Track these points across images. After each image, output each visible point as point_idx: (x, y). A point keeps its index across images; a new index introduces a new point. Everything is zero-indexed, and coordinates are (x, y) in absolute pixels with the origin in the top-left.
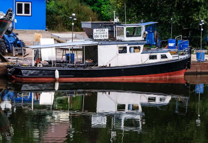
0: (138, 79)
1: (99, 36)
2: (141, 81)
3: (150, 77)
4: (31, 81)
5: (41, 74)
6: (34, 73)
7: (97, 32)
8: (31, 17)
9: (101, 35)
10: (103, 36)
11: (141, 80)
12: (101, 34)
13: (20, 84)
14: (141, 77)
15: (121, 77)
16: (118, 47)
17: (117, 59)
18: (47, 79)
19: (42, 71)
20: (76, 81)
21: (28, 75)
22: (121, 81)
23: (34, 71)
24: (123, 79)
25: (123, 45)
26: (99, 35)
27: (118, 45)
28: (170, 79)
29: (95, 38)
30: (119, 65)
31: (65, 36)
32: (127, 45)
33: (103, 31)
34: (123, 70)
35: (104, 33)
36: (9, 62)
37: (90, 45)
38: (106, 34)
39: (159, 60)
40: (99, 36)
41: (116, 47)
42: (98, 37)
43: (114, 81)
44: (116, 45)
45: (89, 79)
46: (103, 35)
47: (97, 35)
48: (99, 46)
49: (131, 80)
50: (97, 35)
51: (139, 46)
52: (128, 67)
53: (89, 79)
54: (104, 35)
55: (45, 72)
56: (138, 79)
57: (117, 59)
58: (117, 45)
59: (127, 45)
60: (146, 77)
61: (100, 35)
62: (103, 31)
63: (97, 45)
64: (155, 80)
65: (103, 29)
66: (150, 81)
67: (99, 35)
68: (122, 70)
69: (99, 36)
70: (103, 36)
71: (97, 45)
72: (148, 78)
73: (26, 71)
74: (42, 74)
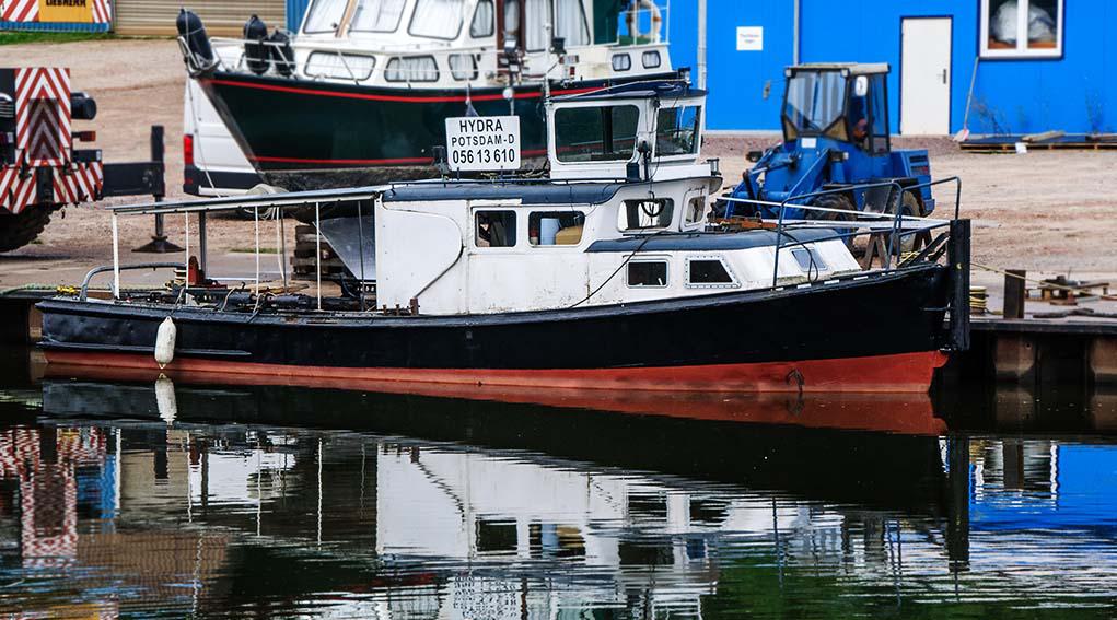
0: (563, 386)
1: (476, 157)
2: (569, 399)
3: (621, 378)
4: (82, 368)
5: (116, 335)
6: (88, 329)
7: (464, 135)
8: (1063, 62)
9: (483, 148)
10: (492, 155)
11: (574, 393)
12: (486, 147)
13: (942, 442)
14: (571, 377)
15: (471, 374)
16: (475, 210)
17: (468, 274)
18: (142, 361)
19: (118, 323)
20: (261, 381)
21: (64, 338)
22: (468, 393)
23: (90, 321)
24: (480, 384)
25: (497, 202)
26: (472, 147)
27: (473, 203)
28: (784, 403)
29: (453, 167)
30: (473, 311)
31: (172, 143)
32: (520, 200)
33: (494, 127)
34: (469, 336)
35: (499, 139)
36: (989, 312)
37: (342, 199)
38: (511, 146)
39: (678, 285)
40: (476, 157)
41: (465, 210)
42: (469, 157)
43: (433, 390)
44: (465, 201)
45: (315, 375)
46: (492, 148)
47: (462, 148)
48: (378, 205)
49: (517, 392)
50: (466, 148)
51: (577, 208)
52: (488, 322)
53: (315, 375)
54: (501, 147)
55: (131, 328)
56: (563, 386)
57: (468, 274)
58: (468, 200)
59: (520, 200)
60: (598, 378)
61: (479, 147)
62: (494, 127)
63: (372, 200)
64: (659, 399)
65: (494, 119)
66: (622, 401)
67: (472, 147)
68: (464, 334)
69: (475, 154)
70: (492, 155)
71: (372, 200)
72: (614, 384)
73: (59, 318)
74: (117, 338)
